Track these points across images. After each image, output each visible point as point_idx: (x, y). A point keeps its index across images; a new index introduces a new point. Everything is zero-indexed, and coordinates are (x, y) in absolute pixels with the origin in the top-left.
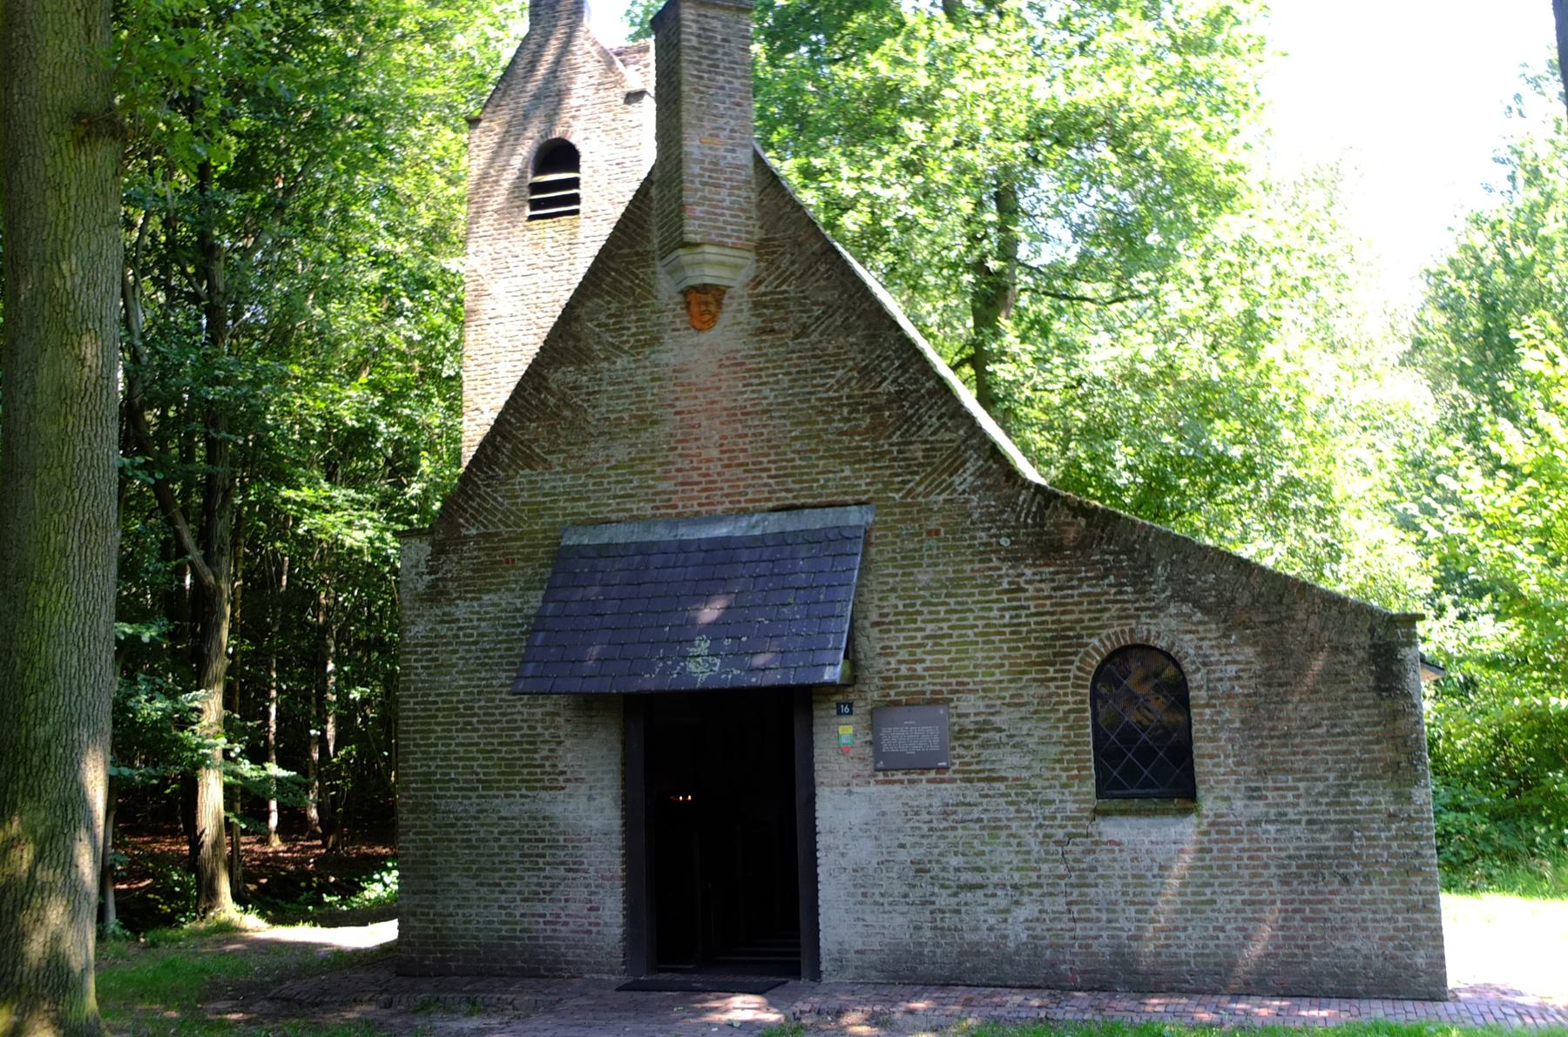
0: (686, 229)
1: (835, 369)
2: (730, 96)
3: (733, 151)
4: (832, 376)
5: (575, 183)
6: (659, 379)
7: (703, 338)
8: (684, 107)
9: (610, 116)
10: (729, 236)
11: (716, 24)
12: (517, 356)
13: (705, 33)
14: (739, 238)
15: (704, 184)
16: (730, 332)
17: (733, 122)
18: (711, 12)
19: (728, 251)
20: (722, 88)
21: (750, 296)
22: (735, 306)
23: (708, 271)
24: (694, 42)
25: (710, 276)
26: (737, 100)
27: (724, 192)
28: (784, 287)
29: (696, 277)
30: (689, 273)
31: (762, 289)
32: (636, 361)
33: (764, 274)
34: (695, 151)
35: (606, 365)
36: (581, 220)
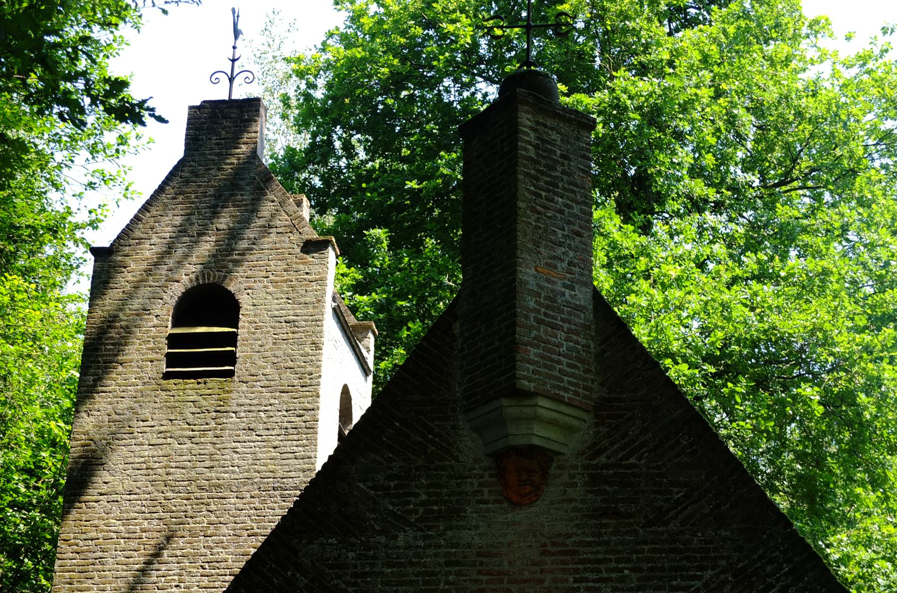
0: (520, 373)
1: (703, 568)
2: (569, 223)
3: (573, 289)
4: (699, 578)
5: (232, 339)
6: (458, 563)
7: (521, 515)
8: (519, 227)
9: (283, 265)
10: (566, 390)
11: (554, 136)
12: (133, 544)
13: (543, 145)
14: (576, 393)
15: (540, 322)
16: (552, 513)
17: (571, 254)
18: (550, 122)
19: (563, 408)
20: (561, 212)
21: (585, 467)
22: (565, 478)
23: (538, 430)
24: (532, 153)
25: (541, 435)
26: (576, 228)
27: (561, 335)
28: (632, 460)
29: (518, 436)
30: (512, 430)
31: (603, 459)
32: (425, 538)
33: (605, 442)
34: (531, 281)
35: (383, 539)
36: (234, 384)
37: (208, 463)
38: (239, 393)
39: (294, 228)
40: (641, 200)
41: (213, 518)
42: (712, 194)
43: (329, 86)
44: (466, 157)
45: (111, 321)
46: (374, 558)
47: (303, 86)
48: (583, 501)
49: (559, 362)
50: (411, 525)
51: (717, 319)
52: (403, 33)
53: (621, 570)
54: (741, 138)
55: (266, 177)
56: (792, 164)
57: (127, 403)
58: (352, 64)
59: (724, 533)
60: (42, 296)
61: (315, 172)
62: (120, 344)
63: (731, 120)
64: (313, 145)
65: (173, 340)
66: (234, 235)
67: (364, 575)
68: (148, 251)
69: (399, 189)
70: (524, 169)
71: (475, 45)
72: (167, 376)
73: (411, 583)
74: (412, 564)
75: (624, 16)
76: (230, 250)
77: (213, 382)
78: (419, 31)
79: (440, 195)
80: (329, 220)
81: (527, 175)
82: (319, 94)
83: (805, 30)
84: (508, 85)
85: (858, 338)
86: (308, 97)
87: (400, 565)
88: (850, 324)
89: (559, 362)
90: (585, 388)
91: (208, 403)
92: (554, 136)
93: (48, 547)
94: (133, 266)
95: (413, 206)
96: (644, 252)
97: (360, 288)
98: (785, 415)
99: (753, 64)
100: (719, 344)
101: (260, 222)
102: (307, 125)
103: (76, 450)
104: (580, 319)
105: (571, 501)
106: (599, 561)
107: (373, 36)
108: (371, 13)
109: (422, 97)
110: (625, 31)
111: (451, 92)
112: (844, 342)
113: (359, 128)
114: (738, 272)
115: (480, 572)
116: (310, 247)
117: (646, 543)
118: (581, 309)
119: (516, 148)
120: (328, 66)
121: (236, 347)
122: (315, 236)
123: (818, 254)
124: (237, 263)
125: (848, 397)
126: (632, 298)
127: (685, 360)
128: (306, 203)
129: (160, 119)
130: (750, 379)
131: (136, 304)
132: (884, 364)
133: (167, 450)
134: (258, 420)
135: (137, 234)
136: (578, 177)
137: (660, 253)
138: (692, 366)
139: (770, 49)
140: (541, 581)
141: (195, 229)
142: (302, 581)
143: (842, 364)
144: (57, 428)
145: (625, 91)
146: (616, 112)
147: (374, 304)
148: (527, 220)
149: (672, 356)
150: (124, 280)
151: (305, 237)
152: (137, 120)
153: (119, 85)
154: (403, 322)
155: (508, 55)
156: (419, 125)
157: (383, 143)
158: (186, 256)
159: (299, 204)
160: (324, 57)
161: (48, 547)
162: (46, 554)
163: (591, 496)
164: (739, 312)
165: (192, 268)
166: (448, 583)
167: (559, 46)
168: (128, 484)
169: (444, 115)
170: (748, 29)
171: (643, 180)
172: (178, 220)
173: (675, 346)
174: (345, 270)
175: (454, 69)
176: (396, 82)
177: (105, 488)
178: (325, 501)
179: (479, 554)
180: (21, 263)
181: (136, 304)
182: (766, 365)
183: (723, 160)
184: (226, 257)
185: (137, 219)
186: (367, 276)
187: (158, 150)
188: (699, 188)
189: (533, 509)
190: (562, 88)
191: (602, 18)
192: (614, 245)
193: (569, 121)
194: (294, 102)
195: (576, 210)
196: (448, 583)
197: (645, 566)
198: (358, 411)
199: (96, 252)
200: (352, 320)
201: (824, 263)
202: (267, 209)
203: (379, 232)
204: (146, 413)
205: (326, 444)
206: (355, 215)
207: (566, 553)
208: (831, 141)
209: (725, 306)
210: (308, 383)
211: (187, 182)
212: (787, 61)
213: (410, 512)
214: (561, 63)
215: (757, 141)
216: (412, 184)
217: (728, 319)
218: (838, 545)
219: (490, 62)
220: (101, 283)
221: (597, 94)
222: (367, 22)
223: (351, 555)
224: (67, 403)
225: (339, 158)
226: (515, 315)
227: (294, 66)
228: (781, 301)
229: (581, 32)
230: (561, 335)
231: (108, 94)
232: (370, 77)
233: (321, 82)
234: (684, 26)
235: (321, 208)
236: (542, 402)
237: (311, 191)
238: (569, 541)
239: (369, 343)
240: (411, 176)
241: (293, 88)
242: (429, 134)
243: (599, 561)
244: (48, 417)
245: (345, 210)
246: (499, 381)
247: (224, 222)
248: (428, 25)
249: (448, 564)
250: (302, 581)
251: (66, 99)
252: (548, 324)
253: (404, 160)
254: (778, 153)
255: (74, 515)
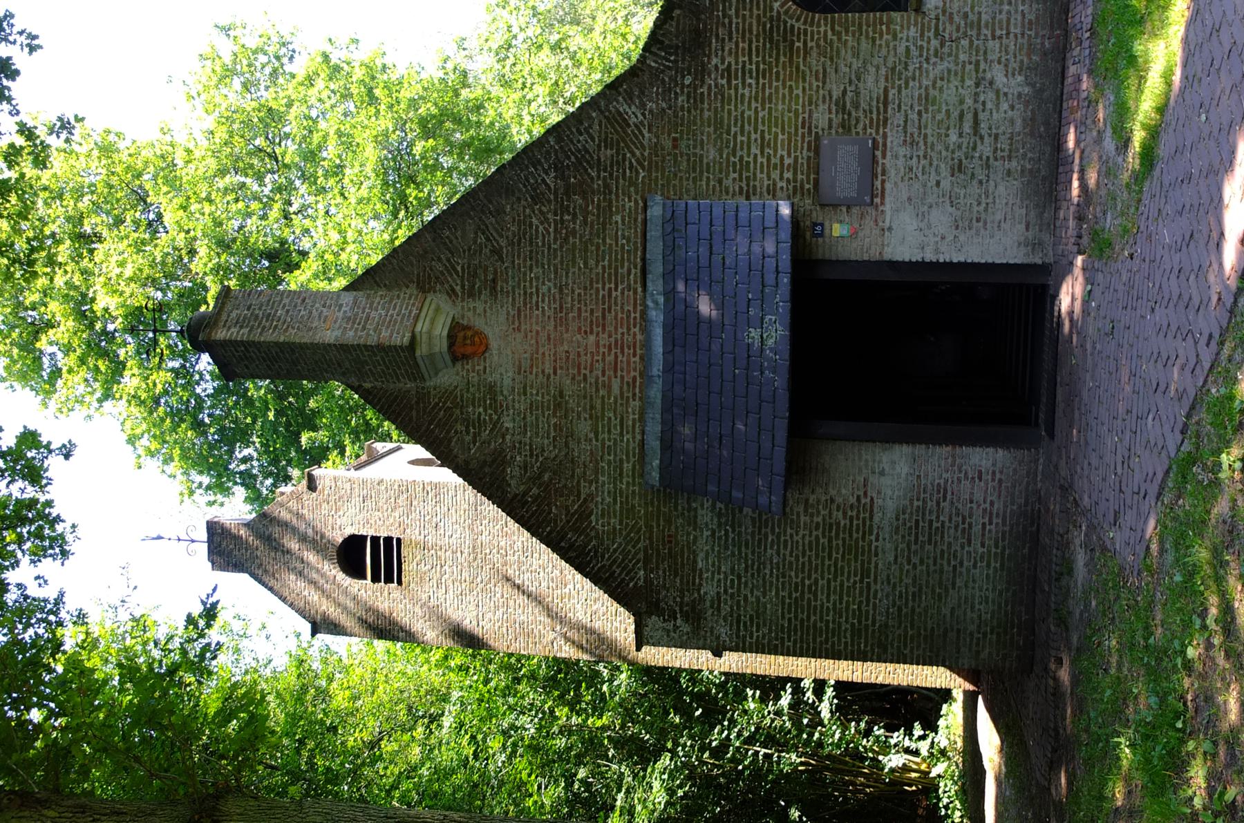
0: (398, 343)
3: (341, 305)
4: (537, 227)
5: (375, 540)
6: (525, 388)
7: (494, 344)
9: (325, 505)
10: (410, 312)
11: (234, 315)
12: (511, 603)
13: (239, 323)
14: (413, 305)
15: (364, 328)
16: (492, 322)
18: (224, 317)
19: (423, 314)
20: (288, 311)
21: (463, 301)
22: (470, 314)
23: (437, 332)
25: (441, 330)
28: (459, 269)
29: (441, 345)
30: (437, 349)
31: (458, 288)
32: (508, 409)
33: (446, 286)
35: (508, 437)
37: (459, 554)
38: (411, 534)
39: (299, 498)
40: (282, 257)
41: (495, 551)
42: (277, 206)
43: (201, 473)
44: (253, 376)
45: (362, 621)
46: (520, 443)
47: (201, 491)
48: (486, 302)
49: (392, 316)
50: (499, 418)
51: (369, 208)
52: (163, 420)
53: (531, 279)
54: (243, 186)
55: (263, 516)
56: (265, 151)
57: (417, 609)
58: (184, 457)
60: (346, 670)
61: (262, 483)
62: (378, 614)
63: (226, 191)
64: (242, 484)
65: (376, 579)
66: (303, 539)
67: (531, 450)
68: (314, 597)
69: (275, 425)
70: (256, 336)
71: (173, 370)
72: (400, 583)
73: (537, 419)
74: (524, 418)
75: (153, 264)
76: (314, 541)
77: (404, 552)
78: (161, 409)
79: (281, 397)
80: (295, 473)
81: (261, 334)
82: (206, 480)
83: (168, 138)
84: (199, 347)
85: (382, 113)
86: (208, 488)
87: (525, 426)
88: (373, 119)
89: (392, 316)
92: (234, 315)
93: (513, 660)
94: (324, 607)
95: (287, 416)
96: (321, 256)
97: (342, 453)
98: (434, 165)
99: (187, 173)
100: (386, 207)
101: (294, 521)
102: (229, 489)
103: (449, 643)
104: (363, 301)
105: (485, 311)
106: (525, 293)
107: (165, 442)
108: (148, 444)
109: (209, 408)
110: (163, 263)
111: (207, 387)
112: (386, 123)
113: (231, 452)
114: (336, 191)
116: (312, 486)
117: (513, 262)
120: (186, 473)
121: (364, 538)
122: (304, 482)
123: (325, 137)
124: (322, 536)
125: (423, 122)
126: (353, 266)
127: (395, 231)
128: (282, 489)
129: (214, 590)
130: (409, 187)
131: (350, 604)
132: (400, 96)
133: (450, 582)
134: (430, 521)
135: (302, 604)
137: (322, 245)
138: (400, 227)
139: (180, 162)
140: (537, 332)
141: (299, 566)
142: (535, 491)
143: (401, 125)
144: (436, 656)
145: (206, 265)
146: (221, 271)
147: (353, 443)
148: (294, 336)
149: (392, 241)
150: (333, 612)
151: (305, 489)
152: (214, 605)
153: (190, 620)
154: (367, 423)
155: (181, 347)
156: (229, 410)
157: (242, 435)
158: (318, 571)
159: (282, 494)
160: (180, 477)
161: (513, 660)
162: (519, 660)
164: (364, 192)
165: (326, 567)
166: (537, 394)
167: (174, 310)
168: (472, 607)
169: (222, 393)
170: (165, 177)
171: (272, 256)
172: (293, 577)
173: (386, 237)
174: (330, 463)
175: (189, 386)
176: (198, 426)
177: (475, 623)
178: (485, 477)
180: (324, 684)
181: (350, 604)
182: (400, 173)
183: (256, 198)
184: (318, 543)
185: (291, 605)
186: (335, 447)
187: (239, 592)
188: (275, 213)
189: (490, 336)
190: (203, 308)
191: (154, 280)
192: (316, 276)
193: (223, 304)
194: (212, 498)
195: (286, 301)
196: (537, 394)
197: (529, 263)
198: (426, 454)
199: (314, 632)
200: (364, 458)
201: (332, 132)
202: (285, 515)
203: (305, 438)
204: (424, 597)
205: (447, 476)
206: (291, 452)
207: (519, 315)
208: (247, 123)
209: (360, 201)
210: (405, 488)
211: (266, 571)
212: (189, 151)
213: (491, 419)
214: (186, 309)
215: (246, 175)
216: (271, 415)
217: (369, 200)
218: (520, 138)
219: (185, 360)
220: (335, 628)
221: (208, 284)
222: (154, 446)
223: (518, 458)
224: (418, 650)
225: (253, 467)
226: (358, 345)
227: (186, 496)
228: (357, 164)
229: (165, 295)
231: (196, 626)
232: (194, 444)
233: (198, 478)
234: (162, 223)
235: (287, 479)
236: (418, 328)
237: (275, 485)
238: (512, 313)
239: (380, 447)
240: (265, 415)
241: (201, 498)
242: (236, 403)
244: (427, 661)
245: (289, 462)
246: (403, 357)
247: (294, 545)
248: (157, 401)
249: (525, 394)
250: (535, 491)
251: (202, 656)
252: (366, 322)
253: (254, 422)
254: (255, 162)
255: (491, 642)
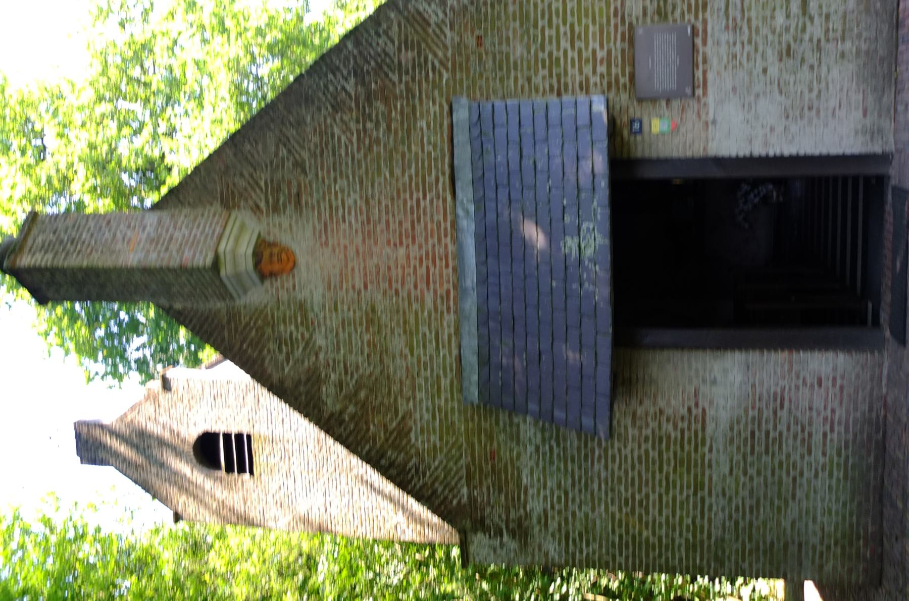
0: (201, 263)
1: (333, 135)
5: (227, 437)
7: (302, 260)
11: (40, 240)
12: (356, 491)
15: (167, 249)
21: (268, 215)
22: (276, 230)
24: (50, 256)
25: (246, 248)
27: (177, 234)
28: (262, 184)
29: (246, 263)
33: (251, 202)
35: (321, 356)
49: (195, 236)
50: (311, 336)
52: (60, 320)
59: (309, 119)
73: (350, 335)
77: (254, 446)
81: (65, 259)
87: (338, 343)
89: (195, 236)
90: (214, 215)
91: (268, 449)
106: (331, 207)
115: (341, 288)
117: (317, 175)
118: (160, 222)
119: (46, 269)
136: (69, 222)
163: (288, 212)
179: (329, 288)
193: (30, 229)
223: (333, 376)
226: (161, 268)
230: (177, 234)
243: (331, 207)
